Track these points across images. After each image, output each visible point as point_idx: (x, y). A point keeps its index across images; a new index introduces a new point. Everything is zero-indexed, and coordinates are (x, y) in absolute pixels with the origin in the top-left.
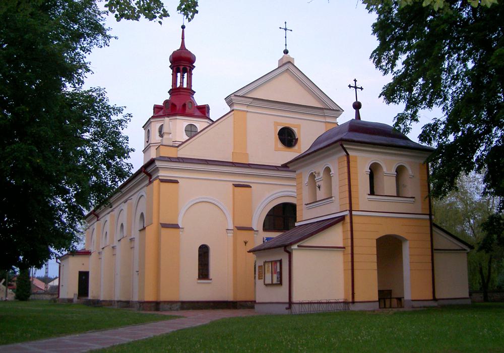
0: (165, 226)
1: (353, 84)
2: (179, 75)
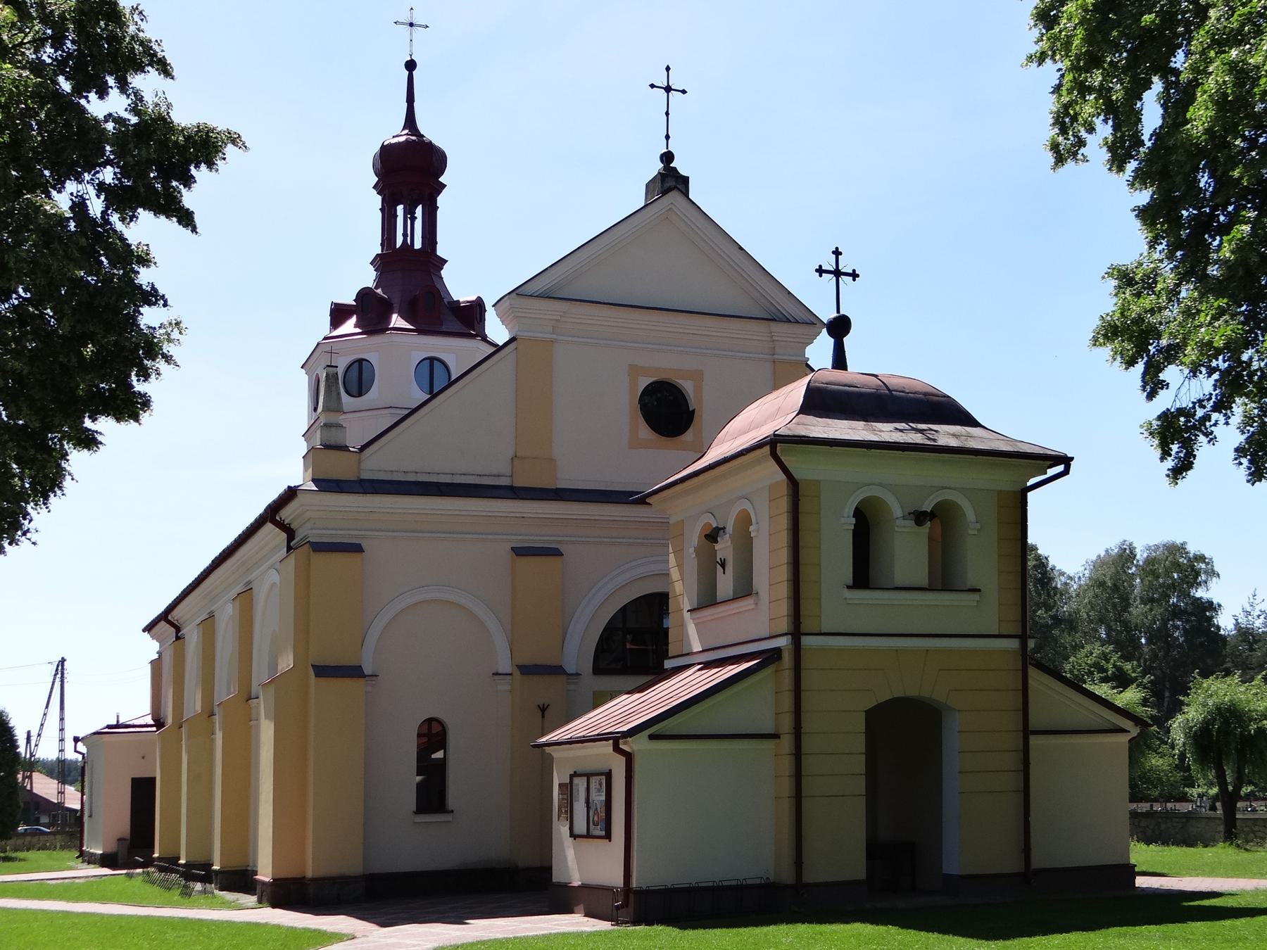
1: (829, 264)
2: (400, 209)
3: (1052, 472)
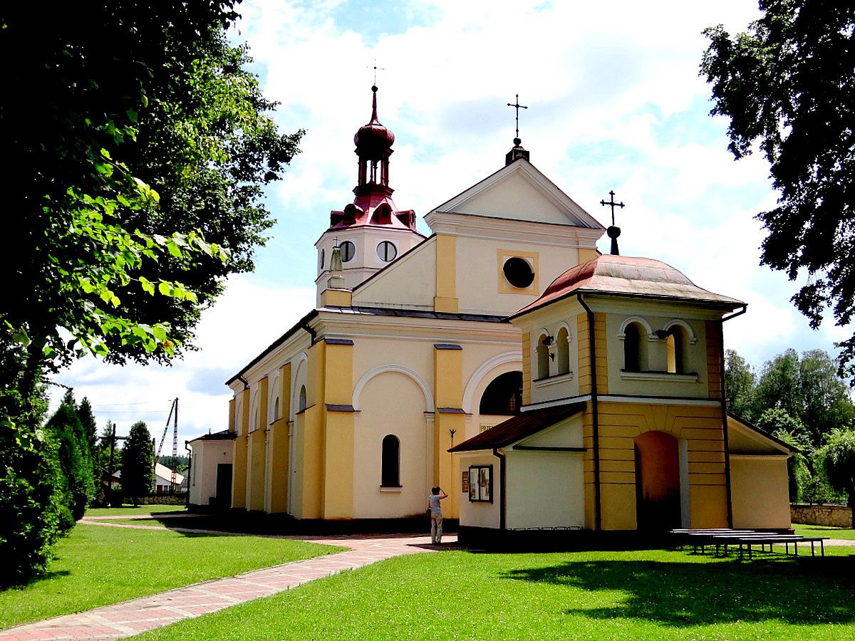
0: (331, 408)
2: (369, 163)
3: (736, 311)
